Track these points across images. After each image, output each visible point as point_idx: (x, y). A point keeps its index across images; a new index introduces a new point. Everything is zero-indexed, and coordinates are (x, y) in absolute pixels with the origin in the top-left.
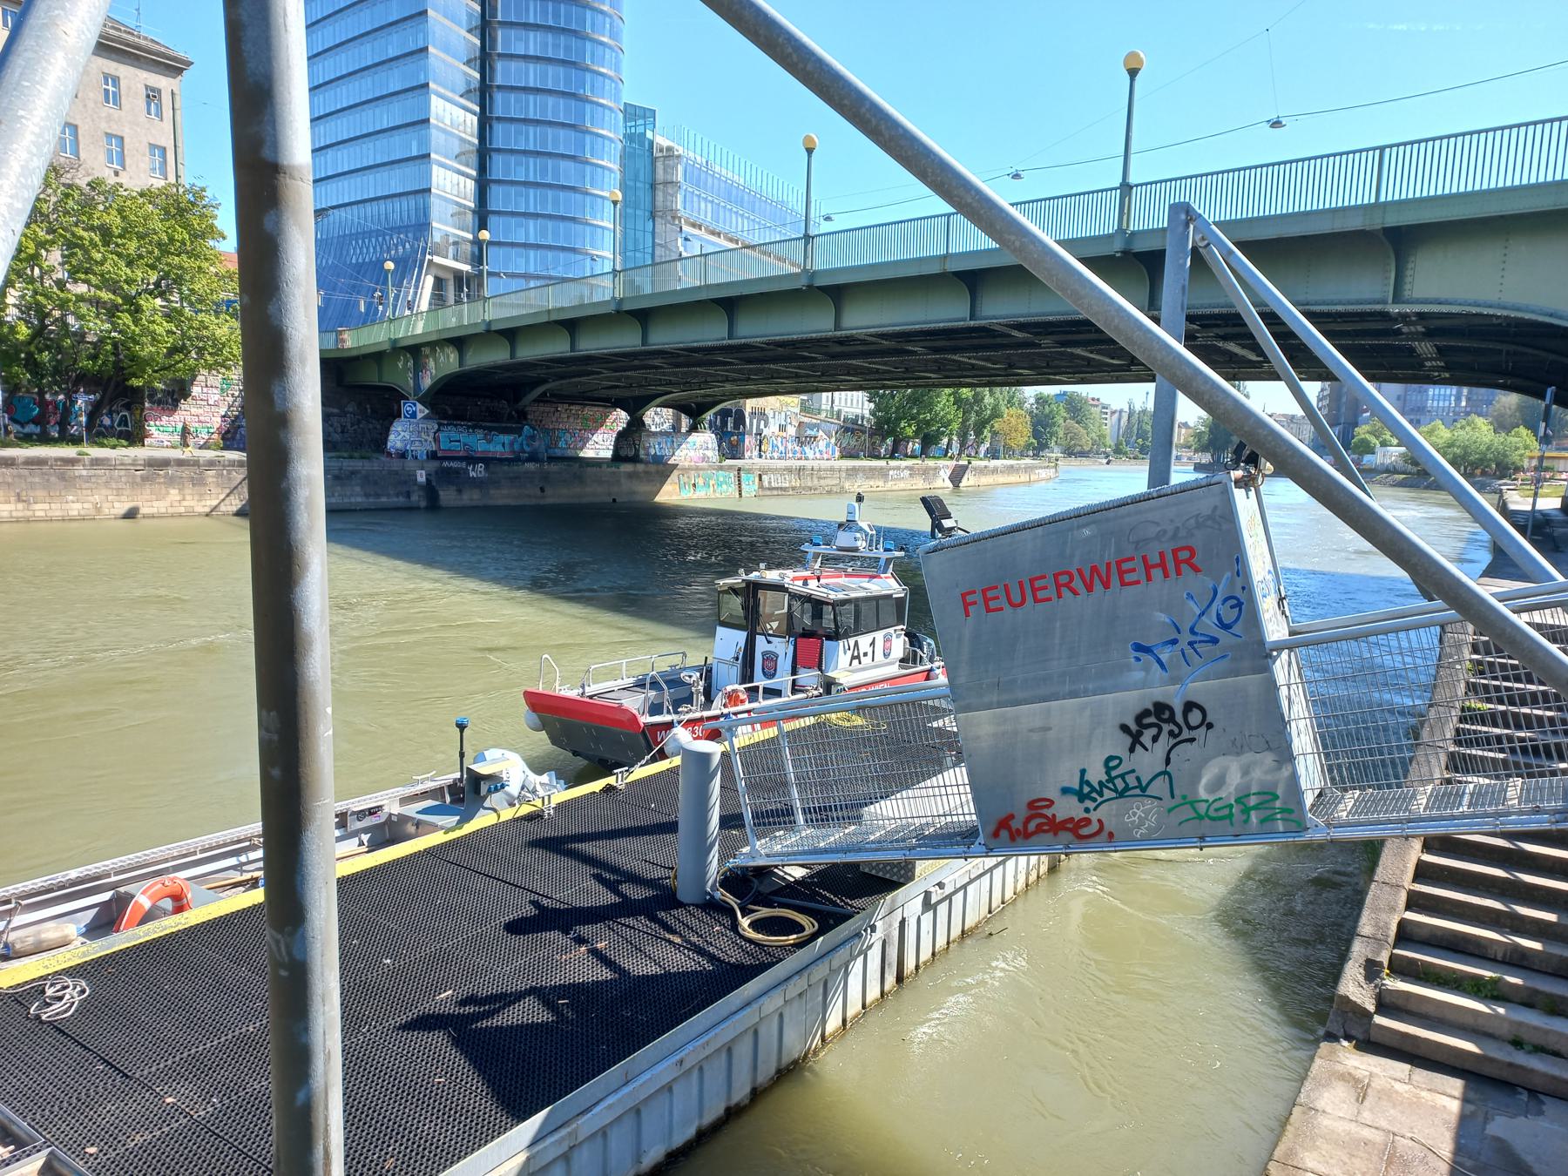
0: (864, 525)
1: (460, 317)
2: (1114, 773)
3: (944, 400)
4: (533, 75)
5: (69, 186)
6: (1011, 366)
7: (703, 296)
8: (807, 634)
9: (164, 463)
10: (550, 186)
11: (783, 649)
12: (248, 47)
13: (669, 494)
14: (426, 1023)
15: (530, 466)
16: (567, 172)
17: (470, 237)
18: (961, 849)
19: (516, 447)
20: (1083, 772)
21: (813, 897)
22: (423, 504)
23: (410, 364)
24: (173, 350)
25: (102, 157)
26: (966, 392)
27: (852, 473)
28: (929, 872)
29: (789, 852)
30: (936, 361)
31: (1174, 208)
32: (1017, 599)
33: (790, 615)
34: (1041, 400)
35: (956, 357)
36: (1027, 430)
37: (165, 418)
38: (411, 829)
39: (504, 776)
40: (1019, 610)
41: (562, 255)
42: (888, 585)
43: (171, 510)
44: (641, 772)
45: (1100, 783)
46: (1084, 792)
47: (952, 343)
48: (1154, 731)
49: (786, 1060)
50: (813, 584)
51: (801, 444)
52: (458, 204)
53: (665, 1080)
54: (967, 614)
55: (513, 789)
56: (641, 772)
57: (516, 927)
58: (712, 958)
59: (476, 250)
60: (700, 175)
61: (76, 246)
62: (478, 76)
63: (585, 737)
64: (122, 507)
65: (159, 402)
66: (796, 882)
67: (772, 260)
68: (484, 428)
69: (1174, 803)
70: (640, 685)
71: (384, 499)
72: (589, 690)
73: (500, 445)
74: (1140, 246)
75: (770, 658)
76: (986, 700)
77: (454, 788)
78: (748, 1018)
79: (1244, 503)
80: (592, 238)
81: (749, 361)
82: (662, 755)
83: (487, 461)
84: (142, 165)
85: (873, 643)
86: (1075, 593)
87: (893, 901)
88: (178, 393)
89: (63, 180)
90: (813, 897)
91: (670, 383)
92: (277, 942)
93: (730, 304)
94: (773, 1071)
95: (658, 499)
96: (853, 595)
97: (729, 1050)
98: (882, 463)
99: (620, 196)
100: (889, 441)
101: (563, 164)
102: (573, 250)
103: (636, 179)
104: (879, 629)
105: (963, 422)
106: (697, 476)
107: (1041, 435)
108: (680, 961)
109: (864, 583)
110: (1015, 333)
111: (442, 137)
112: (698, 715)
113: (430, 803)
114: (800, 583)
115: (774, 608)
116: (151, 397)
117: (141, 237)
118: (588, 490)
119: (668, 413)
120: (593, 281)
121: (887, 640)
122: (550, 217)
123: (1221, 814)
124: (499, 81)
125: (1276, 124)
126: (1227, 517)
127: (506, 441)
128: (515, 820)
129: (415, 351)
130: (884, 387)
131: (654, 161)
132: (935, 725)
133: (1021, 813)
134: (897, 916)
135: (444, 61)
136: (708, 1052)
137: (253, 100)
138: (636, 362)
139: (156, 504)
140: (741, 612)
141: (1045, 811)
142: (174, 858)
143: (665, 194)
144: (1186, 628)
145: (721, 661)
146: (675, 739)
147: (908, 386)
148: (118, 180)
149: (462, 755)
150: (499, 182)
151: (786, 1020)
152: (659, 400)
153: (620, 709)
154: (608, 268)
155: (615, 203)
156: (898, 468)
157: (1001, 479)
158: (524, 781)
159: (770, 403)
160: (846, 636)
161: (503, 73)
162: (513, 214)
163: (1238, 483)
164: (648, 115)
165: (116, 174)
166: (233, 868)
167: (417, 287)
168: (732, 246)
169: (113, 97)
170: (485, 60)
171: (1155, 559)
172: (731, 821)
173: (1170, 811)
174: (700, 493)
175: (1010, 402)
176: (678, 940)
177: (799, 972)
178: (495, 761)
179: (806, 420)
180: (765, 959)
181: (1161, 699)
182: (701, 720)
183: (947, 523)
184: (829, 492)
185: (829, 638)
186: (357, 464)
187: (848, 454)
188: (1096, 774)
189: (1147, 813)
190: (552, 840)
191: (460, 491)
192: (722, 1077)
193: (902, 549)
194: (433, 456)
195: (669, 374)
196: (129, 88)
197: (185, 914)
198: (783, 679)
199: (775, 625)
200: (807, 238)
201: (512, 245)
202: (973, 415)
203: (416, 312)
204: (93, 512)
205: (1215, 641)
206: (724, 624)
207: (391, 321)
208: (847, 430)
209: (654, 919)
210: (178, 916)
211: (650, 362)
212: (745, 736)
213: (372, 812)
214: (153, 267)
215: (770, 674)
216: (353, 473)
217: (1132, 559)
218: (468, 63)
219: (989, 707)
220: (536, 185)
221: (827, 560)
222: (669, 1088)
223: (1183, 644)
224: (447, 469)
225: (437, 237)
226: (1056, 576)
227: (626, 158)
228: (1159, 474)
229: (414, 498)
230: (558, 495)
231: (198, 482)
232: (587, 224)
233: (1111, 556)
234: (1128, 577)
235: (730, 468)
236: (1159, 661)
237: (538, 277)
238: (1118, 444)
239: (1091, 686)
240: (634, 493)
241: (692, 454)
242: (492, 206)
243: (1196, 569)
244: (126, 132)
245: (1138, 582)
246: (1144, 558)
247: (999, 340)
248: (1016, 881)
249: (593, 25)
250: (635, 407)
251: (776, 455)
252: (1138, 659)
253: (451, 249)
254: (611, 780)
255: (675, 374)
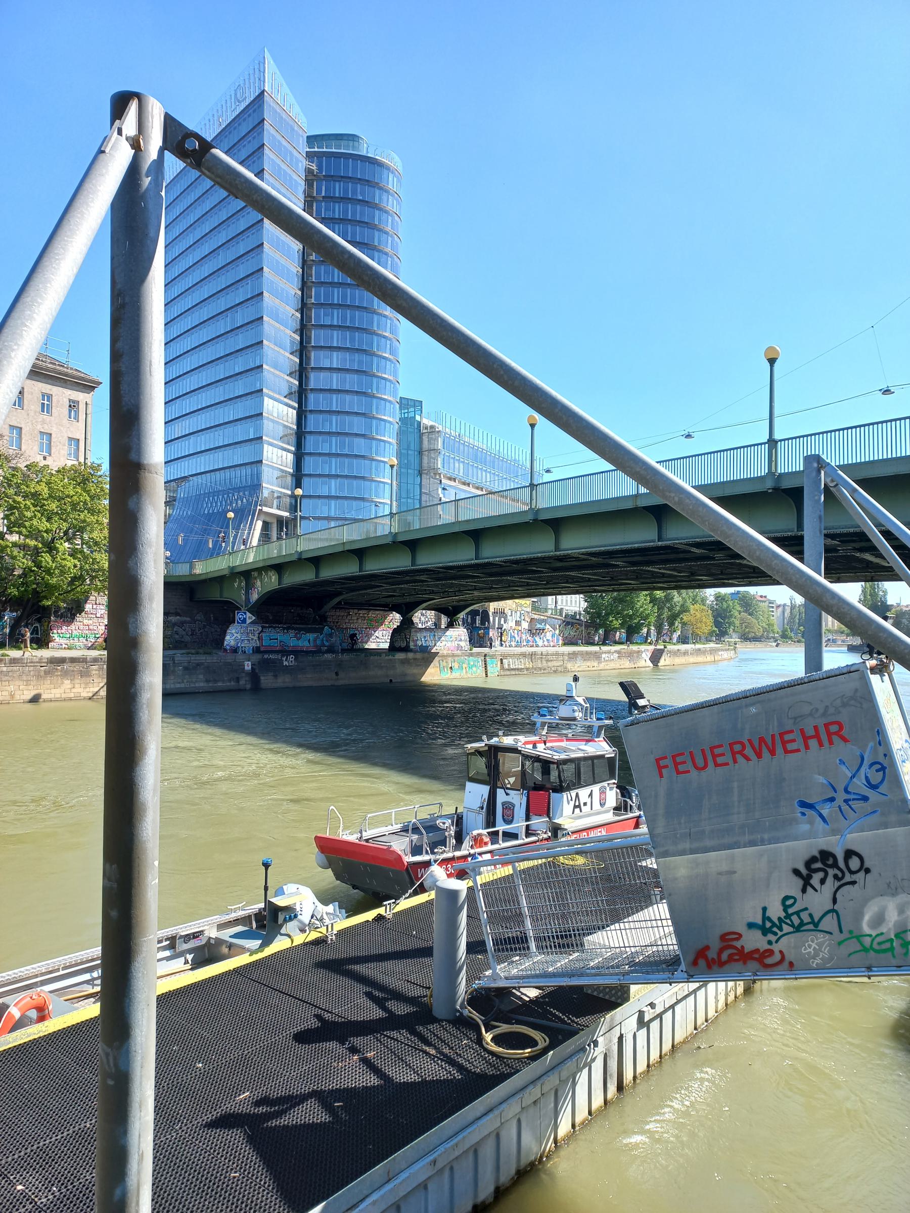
0: (580, 700)
1: (280, 550)
2: (790, 911)
3: (642, 599)
4: (335, 381)
5: (14, 469)
6: (693, 574)
7: (457, 529)
8: (538, 787)
9: (62, 661)
10: (347, 456)
11: (518, 799)
12: (124, 387)
13: (433, 675)
14: (226, 1121)
15: (328, 656)
16: (359, 446)
17: (289, 492)
18: (667, 975)
19: (319, 642)
20: (764, 909)
21: (545, 1015)
22: (248, 686)
23: (243, 584)
24: (74, 579)
25: (36, 448)
26: (659, 594)
27: (573, 656)
28: (641, 994)
29: (525, 974)
30: (634, 571)
31: (808, 459)
32: (701, 763)
33: (523, 772)
34: (718, 597)
35: (650, 569)
36: (710, 621)
37: (65, 628)
38: (225, 950)
39: (298, 909)
40: (703, 773)
41: (354, 503)
42: (602, 747)
43: (64, 696)
44: (405, 904)
45: (779, 919)
46: (766, 927)
47: (646, 558)
48: (821, 875)
49: (524, 1162)
50: (541, 747)
51: (533, 635)
52: (282, 471)
53: (422, 1178)
54: (661, 776)
55: (305, 918)
56: (405, 904)
57: (303, 1037)
58: (461, 1068)
59: (293, 502)
60: (455, 444)
61: (15, 508)
62: (297, 383)
63: (362, 874)
64: (29, 695)
65: (62, 616)
66: (531, 1001)
67: (507, 501)
68: (295, 629)
69: (842, 937)
70: (405, 830)
71: (220, 684)
72: (366, 835)
73: (306, 641)
74: (786, 484)
75: (509, 808)
76: (681, 847)
77: (259, 916)
78: (488, 1125)
79: (880, 686)
80: (376, 490)
81: (491, 575)
82: (422, 889)
83: (297, 652)
84: (62, 452)
85: (591, 795)
86: (748, 759)
87: (612, 1019)
88: (75, 609)
89: (11, 465)
90: (545, 1015)
91: (433, 592)
92: (107, 1055)
93: (476, 534)
94: (513, 1172)
95: (423, 679)
96: (573, 755)
97: (475, 1150)
98: (596, 648)
99: (395, 462)
100: (601, 631)
101: (357, 440)
102: (362, 499)
103: (408, 449)
104: (594, 782)
105: (659, 616)
106: (453, 662)
107: (721, 624)
108: (435, 1071)
109: (582, 745)
110: (694, 550)
111: (271, 424)
112: (450, 855)
113: (240, 928)
114: (530, 746)
115: (511, 766)
116: (56, 612)
117: (60, 499)
118: (371, 673)
119: (431, 614)
120: (375, 520)
121: (603, 792)
122: (346, 477)
123: (884, 947)
124: (312, 385)
125: (887, 392)
126: (866, 700)
127: (310, 640)
128: (305, 944)
129: (247, 575)
130: (595, 591)
131: (421, 435)
132: (644, 864)
133: (715, 945)
134: (616, 1033)
135: (274, 374)
136: (457, 1153)
137: (126, 421)
138: (408, 578)
139: (53, 691)
140: (485, 771)
141: (735, 943)
142: (43, 974)
143: (429, 458)
144: (840, 788)
145: (470, 810)
146: (432, 875)
147: (614, 590)
148: (46, 463)
149: (266, 889)
150: (310, 454)
151: (523, 1124)
152: (424, 605)
153: (389, 851)
154: (387, 512)
155: (392, 466)
156: (609, 652)
157: (692, 659)
158: (314, 912)
159: (508, 605)
160: (569, 789)
161: (315, 380)
162: (320, 476)
163: (873, 670)
164: (417, 405)
165: (45, 458)
166: (87, 982)
167: (250, 529)
168: (479, 492)
169: (46, 407)
170: (302, 372)
171: (810, 732)
172: (475, 947)
173: (839, 943)
174: (456, 674)
175: (694, 601)
176: (433, 1052)
177: (533, 1082)
178: (291, 895)
179: (536, 617)
180: (506, 1070)
181: (825, 848)
182: (452, 859)
183: (641, 702)
184: (555, 672)
185: (556, 790)
186: (202, 658)
187: (568, 642)
188: (775, 912)
189: (820, 945)
190: (334, 961)
191: (276, 676)
192: (470, 1175)
193: (611, 718)
194: (257, 650)
195: (432, 586)
196: (58, 401)
197: (46, 1023)
198: (519, 825)
199: (512, 780)
200: (532, 486)
201: (319, 497)
202: (666, 610)
203: (250, 547)
204: (8, 698)
205: (865, 799)
206: (472, 780)
207: (230, 554)
208: (568, 623)
209: (413, 1032)
210: (41, 1024)
211: (418, 578)
212: (487, 875)
213: (195, 936)
214: (65, 521)
215: (508, 820)
216: (198, 665)
217: (792, 731)
218: (290, 375)
219: (682, 853)
220: (338, 455)
221: (553, 727)
222: (424, 1186)
223: (839, 801)
224: (266, 660)
225: (266, 493)
226: (731, 745)
227: (401, 434)
228: (813, 660)
229: (242, 682)
230: (349, 678)
231: (85, 674)
232: (373, 481)
233: (774, 729)
234: (790, 747)
235: (478, 654)
236: (821, 816)
237: (337, 519)
238: (784, 631)
239: (766, 836)
240: (406, 675)
241: (449, 644)
242: (306, 471)
243: (845, 740)
244: (54, 431)
245: (798, 750)
246: (802, 731)
247: (681, 556)
248: (717, 1001)
249: (378, 345)
250: (407, 610)
251: (513, 644)
252: (803, 814)
253: (275, 503)
254: (381, 911)
255: (437, 586)
